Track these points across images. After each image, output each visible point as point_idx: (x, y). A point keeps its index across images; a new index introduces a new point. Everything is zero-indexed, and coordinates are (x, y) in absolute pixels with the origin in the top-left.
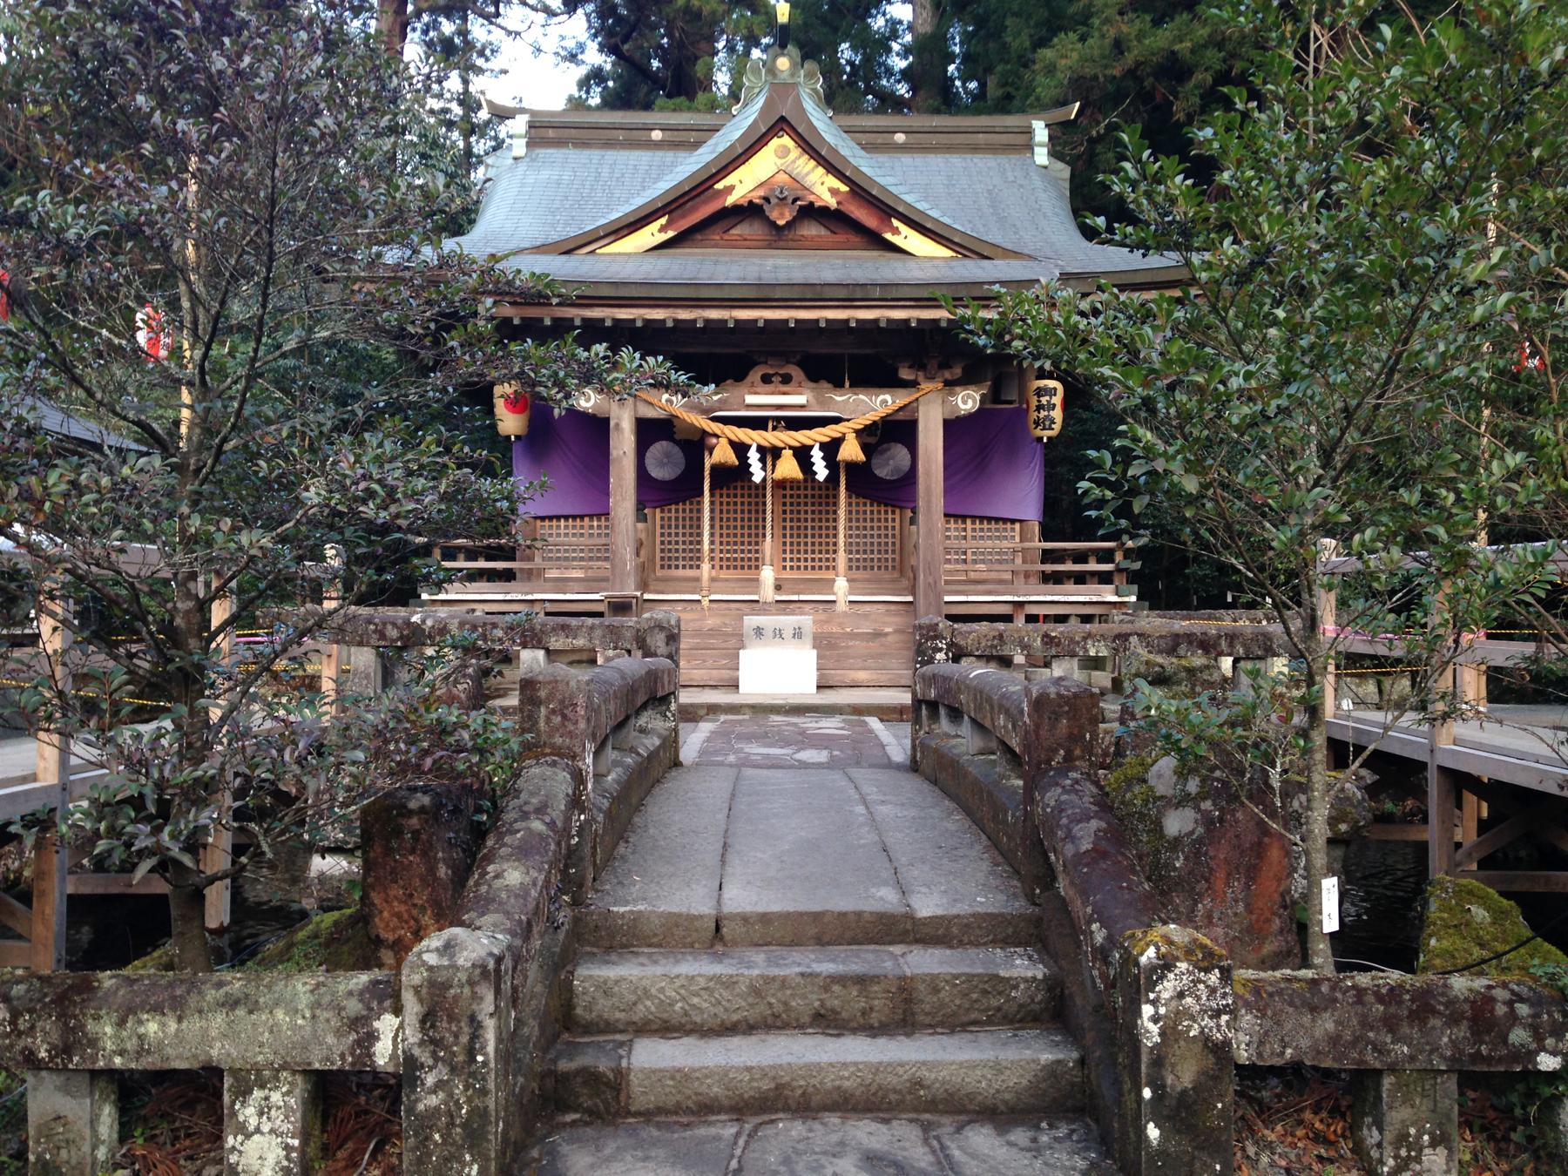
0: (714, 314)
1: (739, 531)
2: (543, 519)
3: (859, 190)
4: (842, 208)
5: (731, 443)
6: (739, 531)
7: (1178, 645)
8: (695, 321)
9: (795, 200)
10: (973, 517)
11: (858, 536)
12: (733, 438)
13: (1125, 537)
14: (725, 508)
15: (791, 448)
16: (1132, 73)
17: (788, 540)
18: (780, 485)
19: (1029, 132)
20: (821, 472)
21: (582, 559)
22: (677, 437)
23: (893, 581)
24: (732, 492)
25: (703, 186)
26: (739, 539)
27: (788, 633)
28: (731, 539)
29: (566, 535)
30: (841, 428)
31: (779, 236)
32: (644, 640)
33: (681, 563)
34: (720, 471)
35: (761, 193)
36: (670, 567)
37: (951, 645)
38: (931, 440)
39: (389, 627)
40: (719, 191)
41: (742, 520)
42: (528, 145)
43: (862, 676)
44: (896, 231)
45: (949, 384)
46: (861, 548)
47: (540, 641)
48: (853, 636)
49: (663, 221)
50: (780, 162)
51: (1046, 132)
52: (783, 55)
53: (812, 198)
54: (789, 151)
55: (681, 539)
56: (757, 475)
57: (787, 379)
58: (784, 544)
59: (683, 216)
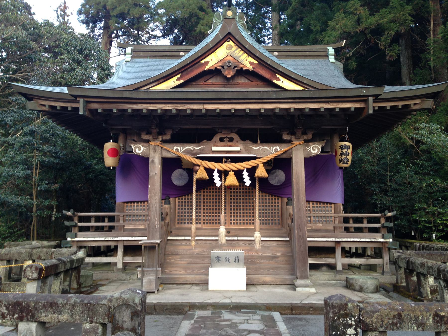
0: (195, 107)
1: (211, 207)
2: (127, 203)
3: (262, 62)
4: (255, 70)
5: (205, 169)
6: (211, 207)
8: (186, 110)
9: (235, 67)
10: (313, 202)
11: (263, 210)
12: (206, 166)
15: (233, 171)
16: (363, 32)
17: (233, 211)
18: (229, 188)
19: (327, 51)
20: (248, 182)
22: (183, 167)
23: (279, 229)
24: (208, 191)
26: (211, 211)
27: (232, 260)
28: (208, 211)
29: (137, 209)
30: (256, 161)
32: (114, 316)
33: (186, 221)
34: (200, 182)
36: (181, 223)
37: (359, 322)
40: (203, 64)
41: (213, 202)
42: (132, 57)
43: (268, 279)
44: (278, 79)
45: (307, 142)
46: (264, 215)
47: (33, 316)
48: (262, 257)
49: (179, 76)
50: (228, 51)
51: (333, 50)
52: (230, 10)
53: (242, 66)
56: (218, 183)
57: (231, 140)
59: (187, 74)
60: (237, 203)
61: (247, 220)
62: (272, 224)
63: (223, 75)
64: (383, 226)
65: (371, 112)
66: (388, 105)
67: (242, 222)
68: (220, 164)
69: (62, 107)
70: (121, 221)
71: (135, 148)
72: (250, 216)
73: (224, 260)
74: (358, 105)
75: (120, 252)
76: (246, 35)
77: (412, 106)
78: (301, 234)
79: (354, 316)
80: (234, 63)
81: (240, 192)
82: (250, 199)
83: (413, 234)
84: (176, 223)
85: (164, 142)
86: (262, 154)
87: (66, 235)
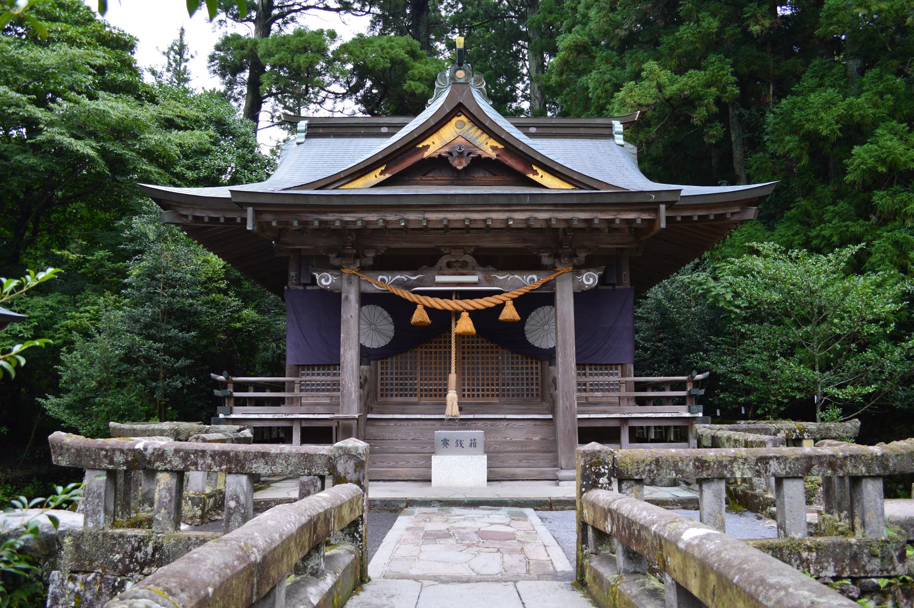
3: (510, 147)
5: (426, 308)
7: (812, 466)
9: (469, 154)
12: (427, 304)
13: (694, 372)
14: (424, 355)
15: (468, 311)
17: (466, 377)
19: (611, 127)
21: (328, 390)
25: (411, 145)
26: (433, 377)
27: (466, 443)
30: (502, 297)
31: (460, 178)
35: (447, 149)
36: (387, 395)
38: (566, 305)
39: (118, 453)
42: (307, 137)
44: (536, 173)
47: (243, 467)
49: (383, 168)
50: (458, 131)
53: (480, 152)
54: (465, 124)
55: (394, 376)
58: (464, 369)
59: (396, 165)
60: (473, 363)
61: (488, 390)
62: (528, 395)
63: (451, 165)
64: (690, 395)
65: (663, 225)
66: (696, 214)
67: (480, 393)
68: (449, 301)
69: (211, 219)
70: (297, 391)
71: (321, 278)
72: (493, 385)
73: (455, 445)
74: (646, 216)
75: (296, 436)
76: (486, 107)
77: (728, 216)
78: (567, 404)
79: (607, 464)
80: (468, 147)
81: (478, 390)
82: (492, 358)
83: (743, 412)
84: (379, 395)
85: (363, 269)
86: (510, 287)
87: (216, 409)
